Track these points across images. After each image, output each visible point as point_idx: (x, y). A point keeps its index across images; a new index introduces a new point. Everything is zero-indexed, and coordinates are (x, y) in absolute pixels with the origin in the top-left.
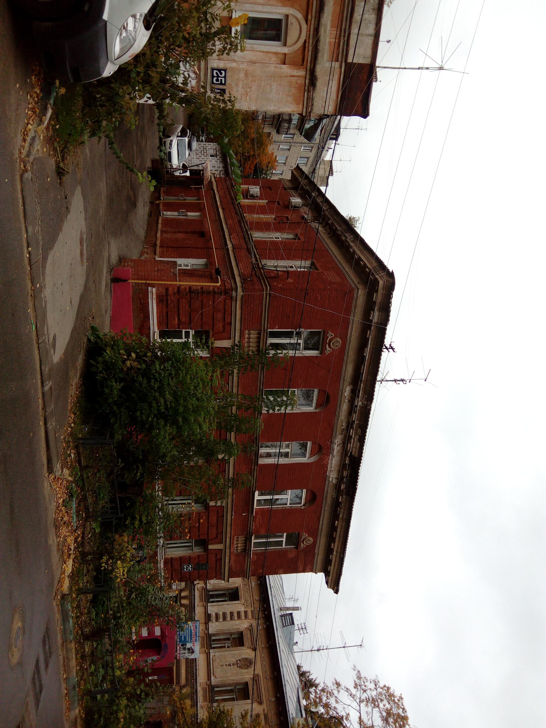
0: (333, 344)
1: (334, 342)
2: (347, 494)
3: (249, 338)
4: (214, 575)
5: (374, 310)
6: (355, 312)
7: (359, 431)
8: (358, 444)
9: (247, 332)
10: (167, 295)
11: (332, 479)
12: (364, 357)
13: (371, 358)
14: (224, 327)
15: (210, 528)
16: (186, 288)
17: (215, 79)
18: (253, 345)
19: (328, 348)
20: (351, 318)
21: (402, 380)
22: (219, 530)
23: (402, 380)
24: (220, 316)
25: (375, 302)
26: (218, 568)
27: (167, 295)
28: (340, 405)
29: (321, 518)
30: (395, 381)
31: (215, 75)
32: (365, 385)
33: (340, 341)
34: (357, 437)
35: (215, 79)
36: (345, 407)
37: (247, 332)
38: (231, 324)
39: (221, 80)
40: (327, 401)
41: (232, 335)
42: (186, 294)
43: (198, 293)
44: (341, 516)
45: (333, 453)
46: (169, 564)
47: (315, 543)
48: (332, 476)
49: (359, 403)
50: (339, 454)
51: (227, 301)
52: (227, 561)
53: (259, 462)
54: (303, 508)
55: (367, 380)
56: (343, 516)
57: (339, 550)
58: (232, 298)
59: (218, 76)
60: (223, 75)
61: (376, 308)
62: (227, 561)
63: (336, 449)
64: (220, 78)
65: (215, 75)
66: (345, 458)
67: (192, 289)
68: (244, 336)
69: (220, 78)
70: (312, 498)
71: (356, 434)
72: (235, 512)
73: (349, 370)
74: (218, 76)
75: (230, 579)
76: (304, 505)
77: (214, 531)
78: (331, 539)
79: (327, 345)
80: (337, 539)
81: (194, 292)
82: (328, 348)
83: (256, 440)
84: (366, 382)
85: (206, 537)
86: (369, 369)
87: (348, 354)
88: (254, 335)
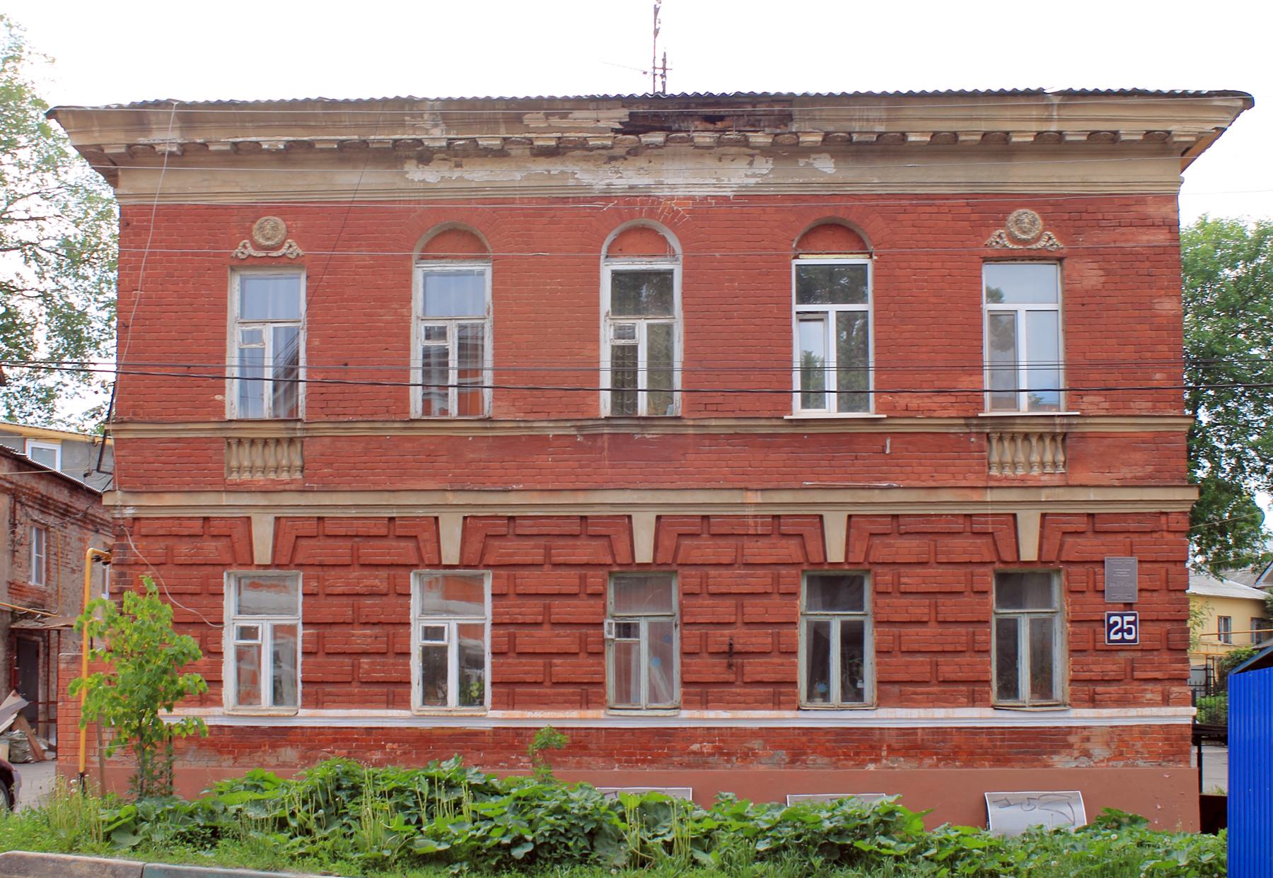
1: (264, 236)
2: (787, 118)
9: (234, 477)
12: (290, 146)
17: (1127, 637)
18: (272, 456)
19: (283, 251)
24: (184, 550)
26: (1132, 526)
28: (476, 189)
31: (1119, 637)
32: (375, 126)
34: (555, 121)
35: (1127, 637)
36: (478, 175)
39: (1129, 623)
44: (880, 128)
45: (648, 186)
46: (1099, 689)
47: (1031, 201)
48: (736, 177)
51: (144, 531)
52: (1093, 495)
53: (608, 414)
55: (357, 126)
56: (880, 120)
57: (1035, 113)
59: (1121, 630)
60: (1118, 619)
61: (142, 140)
62: (1093, 495)
63: (628, 178)
64: (1126, 627)
65: (1119, 637)
66: (648, 146)
74: (1121, 630)
78: (998, 146)
82: (283, 251)
85: (988, 570)
88: (243, 457)
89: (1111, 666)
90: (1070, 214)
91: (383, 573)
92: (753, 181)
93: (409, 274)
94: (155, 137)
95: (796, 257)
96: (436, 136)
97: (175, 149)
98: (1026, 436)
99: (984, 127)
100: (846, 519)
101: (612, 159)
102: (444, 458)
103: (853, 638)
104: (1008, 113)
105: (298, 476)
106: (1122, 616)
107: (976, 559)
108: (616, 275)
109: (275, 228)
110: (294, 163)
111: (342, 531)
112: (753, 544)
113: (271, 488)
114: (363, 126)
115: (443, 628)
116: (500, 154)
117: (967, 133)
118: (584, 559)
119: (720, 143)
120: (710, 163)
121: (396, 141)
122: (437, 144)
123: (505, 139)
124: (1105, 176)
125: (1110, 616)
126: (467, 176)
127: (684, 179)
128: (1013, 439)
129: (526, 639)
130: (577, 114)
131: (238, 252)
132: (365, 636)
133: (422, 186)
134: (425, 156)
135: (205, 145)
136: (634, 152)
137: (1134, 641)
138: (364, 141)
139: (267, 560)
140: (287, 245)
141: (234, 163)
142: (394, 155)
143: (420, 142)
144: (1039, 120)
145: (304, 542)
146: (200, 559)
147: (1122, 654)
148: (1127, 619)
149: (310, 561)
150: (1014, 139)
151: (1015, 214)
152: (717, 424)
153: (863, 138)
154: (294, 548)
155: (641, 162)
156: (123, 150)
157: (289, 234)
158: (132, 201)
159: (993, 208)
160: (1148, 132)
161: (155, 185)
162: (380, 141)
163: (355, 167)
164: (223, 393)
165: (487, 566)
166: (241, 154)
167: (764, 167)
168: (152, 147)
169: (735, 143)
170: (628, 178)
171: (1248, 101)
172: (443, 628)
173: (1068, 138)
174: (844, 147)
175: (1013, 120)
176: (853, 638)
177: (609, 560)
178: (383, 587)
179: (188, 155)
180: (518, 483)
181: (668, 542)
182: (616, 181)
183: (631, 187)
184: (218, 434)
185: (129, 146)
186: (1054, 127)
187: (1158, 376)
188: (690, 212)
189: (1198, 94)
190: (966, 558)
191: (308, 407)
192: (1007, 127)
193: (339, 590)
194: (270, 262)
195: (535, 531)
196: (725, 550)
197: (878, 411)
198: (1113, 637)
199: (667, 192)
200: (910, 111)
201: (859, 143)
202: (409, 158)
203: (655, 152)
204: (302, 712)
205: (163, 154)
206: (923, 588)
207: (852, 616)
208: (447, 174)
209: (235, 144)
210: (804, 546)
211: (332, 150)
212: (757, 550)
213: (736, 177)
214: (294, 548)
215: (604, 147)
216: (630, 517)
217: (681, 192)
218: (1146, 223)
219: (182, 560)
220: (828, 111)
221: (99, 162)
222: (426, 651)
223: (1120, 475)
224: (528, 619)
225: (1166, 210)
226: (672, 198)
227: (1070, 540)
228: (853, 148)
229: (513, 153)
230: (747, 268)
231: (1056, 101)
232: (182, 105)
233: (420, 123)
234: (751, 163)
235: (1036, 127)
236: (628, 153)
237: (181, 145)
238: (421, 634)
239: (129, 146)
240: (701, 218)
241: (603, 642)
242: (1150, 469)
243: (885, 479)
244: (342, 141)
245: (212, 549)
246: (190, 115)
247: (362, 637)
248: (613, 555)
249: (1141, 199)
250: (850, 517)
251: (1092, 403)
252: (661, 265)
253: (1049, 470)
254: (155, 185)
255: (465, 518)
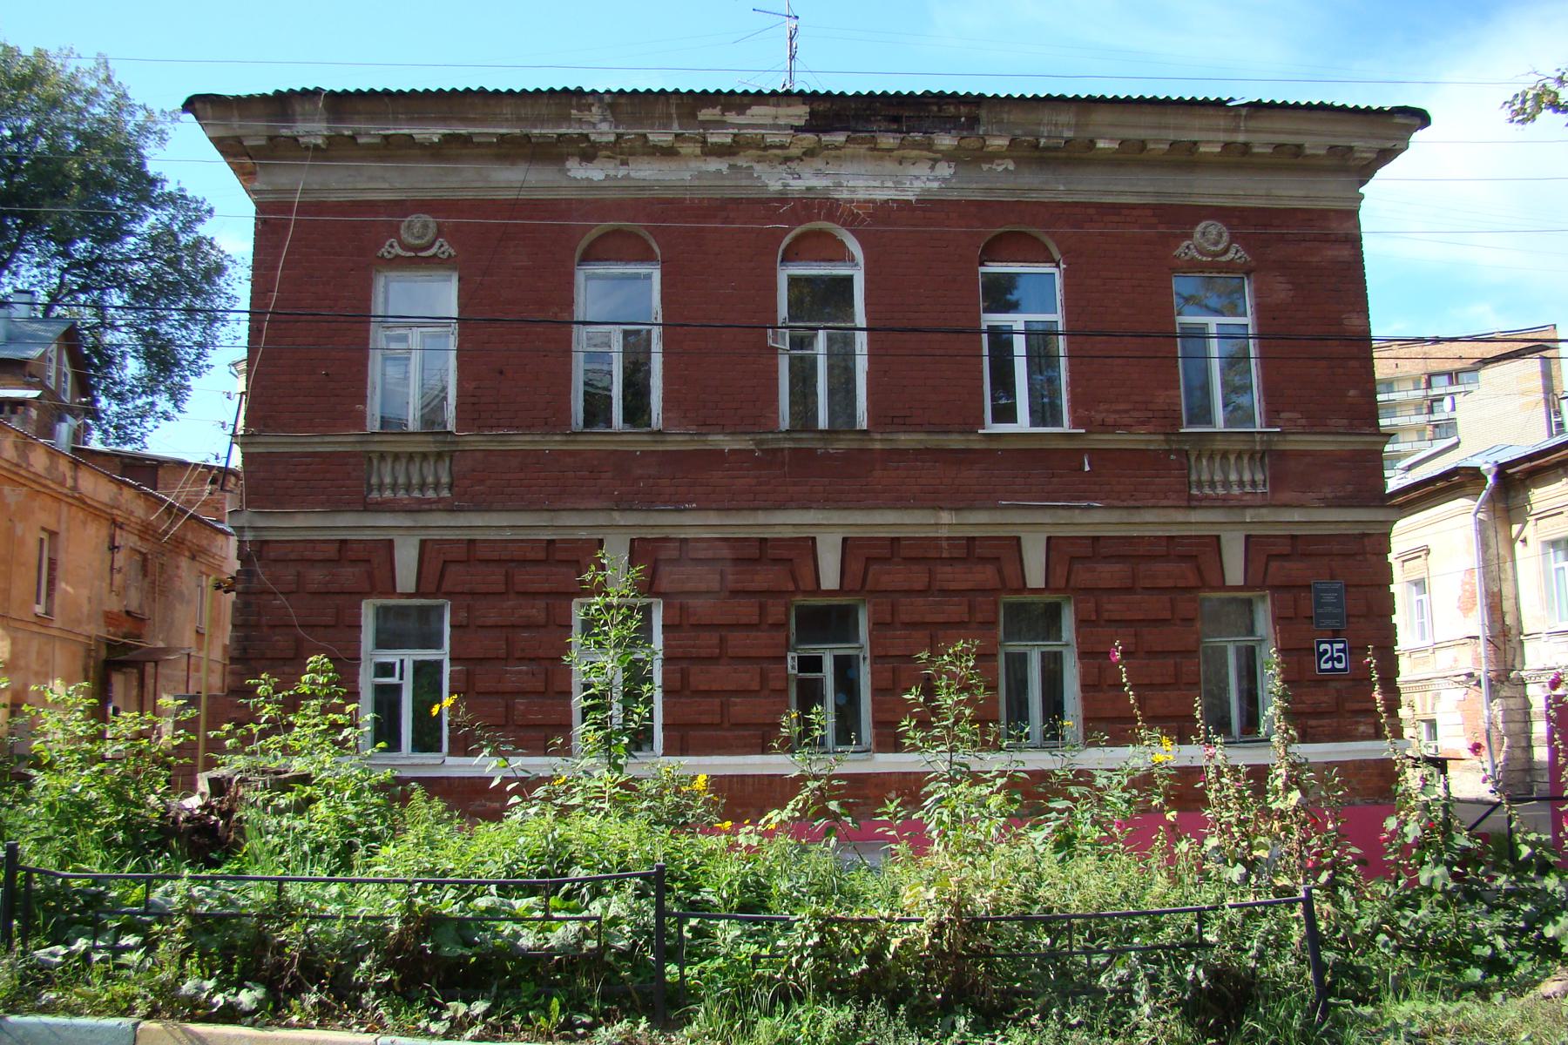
7: (706, 114)
9: (375, 495)
11: (936, 179)
12: (447, 139)
13: (443, 120)
14: (354, 562)
16: (233, 673)
17: (1338, 666)
19: (1230, 255)
24: (317, 576)
28: (642, 188)
31: (1329, 665)
32: (540, 121)
34: (731, 117)
36: (646, 172)
37: (375, 495)
38: (472, 542)
40: (1015, 232)
43: (247, 638)
44: (1068, 134)
46: (1312, 722)
51: (272, 555)
53: (865, 427)
54: (1063, 266)
55: (519, 119)
59: (1331, 658)
60: (1327, 646)
61: (285, 132)
65: (1329, 665)
67: (236, 654)
71: (721, 124)
73: (512, 179)
74: (1331, 658)
76: (1058, 266)
78: (1185, 158)
79: (1223, 259)
82: (1230, 255)
89: (1324, 698)
90: (1247, 223)
91: (541, 603)
92: (935, 185)
93: (572, 275)
94: (300, 128)
95: (982, 264)
96: (604, 132)
97: (320, 141)
98: (1225, 455)
99: (1172, 136)
100: (1044, 542)
101: (787, 159)
102: (610, 474)
103: (845, 667)
104: (1197, 123)
105: (445, 493)
106: (1331, 643)
107: (1181, 584)
108: (794, 281)
109: (425, 226)
110: (447, 159)
111: (495, 555)
112: (949, 569)
113: (415, 507)
114: (526, 119)
115: (415, 662)
116: (669, 152)
117: (1156, 141)
118: (765, 586)
119: (901, 146)
120: (890, 166)
121: (560, 135)
122: (605, 139)
123: (677, 135)
124: (1288, 192)
125: (1319, 643)
126: (632, 174)
127: (864, 180)
128: (1211, 458)
129: (701, 677)
130: (755, 110)
131: (384, 251)
132: (520, 672)
133: (585, 184)
134: (589, 152)
135: (353, 138)
136: (810, 153)
137: (1345, 669)
138: (527, 136)
139: (411, 588)
140: (437, 244)
141: (381, 159)
142: (550, 152)
143: (586, 136)
144: (1225, 131)
145: (452, 568)
147: (1333, 684)
148: (1336, 646)
149: (458, 589)
150: (1202, 149)
151: (1203, 224)
152: (907, 440)
153: (1053, 142)
154: (442, 575)
155: (818, 163)
156: (263, 143)
157: (439, 234)
158: (270, 197)
159: (1184, 217)
160: (1331, 147)
161: (299, 181)
162: (542, 136)
163: (513, 164)
164: (364, 403)
165: (448, 595)
166: (393, 149)
167: (945, 170)
168: (295, 139)
169: (916, 145)
170: (808, 180)
171: (1421, 118)
172: (415, 662)
173: (1256, 150)
174: (1034, 155)
175: (1201, 129)
176: (845, 667)
177: (791, 587)
178: (542, 618)
179: (336, 149)
180: (690, 502)
181: (856, 567)
182: (792, 182)
183: (809, 189)
184: (358, 448)
185: (271, 138)
186: (1241, 138)
187: (1352, 393)
188: (870, 215)
189: (1380, 111)
190: (1170, 583)
191: (458, 417)
192: (1195, 137)
193: (490, 621)
194: (417, 261)
195: (710, 554)
196: (918, 577)
197: (1075, 424)
198: (1324, 666)
199: (845, 195)
200: (1100, 117)
201: (1046, 149)
202: (573, 155)
203: (833, 153)
204: (450, 760)
205: (307, 148)
206: (1128, 616)
207: (844, 649)
208: (612, 173)
209: (386, 137)
210: (1000, 571)
211: (490, 144)
212: (951, 576)
213: (920, 180)
214: (442, 575)
215: (782, 147)
216: (814, 539)
217: (861, 195)
218: (1326, 239)
219: (314, 587)
220: (1015, 116)
221: (235, 156)
222: (379, 689)
223: (1321, 495)
224: (704, 653)
225: (1347, 226)
226: (852, 201)
227: (1274, 565)
228: (1037, 154)
229: (682, 151)
230: (934, 275)
231: (1244, 112)
232: (332, 94)
233: (586, 116)
234: (932, 168)
235: (1224, 137)
236: (805, 154)
237: (328, 137)
238: (372, 670)
239: (271, 138)
240: (878, 223)
241: (787, 677)
242: (1350, 488)
243: (1086, 499)
244: (502, 135)
245: (349, 575)
246: (341, 103)
247: (517, 675)
248: (795, 581)
249: (1323, 214)
250: (1049, 539)
251: (1289, 420)
252: (841, 271)
253: (1248, 489)
254: (299, 181)
255: (632, 541)
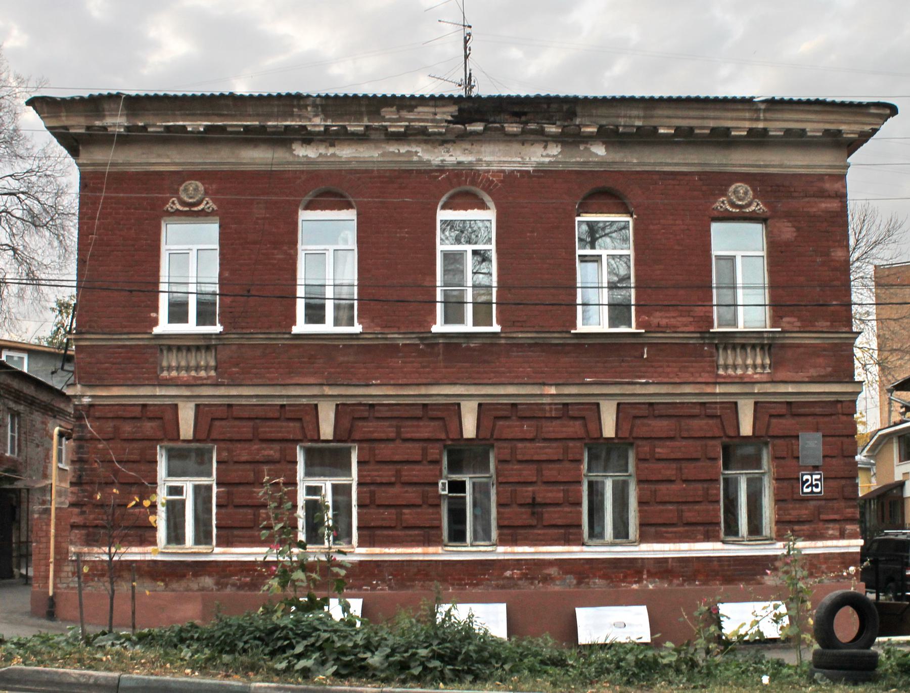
0: (740, 200)
2: (572, 115)
3: (178, 368)
4: (844, 418)
5: (105, 128)
6: (122, 164)
8: (420, 109)
9: (165, 374)
10: (84, 526)
12: (208, 129)
13: (206, 116)
14: (150, 419)
15: (685, 434)
19: (752, 208)
20: (108, 169)
21: (466, 42)
22: (696, 411)
23: (466, 42)
24: (127, 428)
25: (88, 128)
27: (84, 526)
29: (666, 169)
30: (466, 57)
32: (270, 116)
33: (733, 187)
36: (346, 153)
38: (144, 406)
39: (816, 480)
41: (168, 402)
42: (83, 491)
44: (639, 123)
45: (470, 163)
48: (538, 156)
49: (317, 123)
50: (476, 148)
52: (790, 389)
55: (258, 115)
56: (638, 117)
58: (91, 406)
62: (790, 389)
64: (814, 483)
68: (172, 379)
69: (814, 483)
70: (605, 193)
72: (640, 377)
73: (257, 157)
75: (857, 378)
76: (632, 216)
77: (696, 423)
79: (196, 209)
80: (712, 124)
81: (80, 477)
82: (752, 208)
83: (426, 338)
84: (263, 115)
85: (718, 443)
86: (231, 115)
87: (215, 164)
146: (138, 436)
